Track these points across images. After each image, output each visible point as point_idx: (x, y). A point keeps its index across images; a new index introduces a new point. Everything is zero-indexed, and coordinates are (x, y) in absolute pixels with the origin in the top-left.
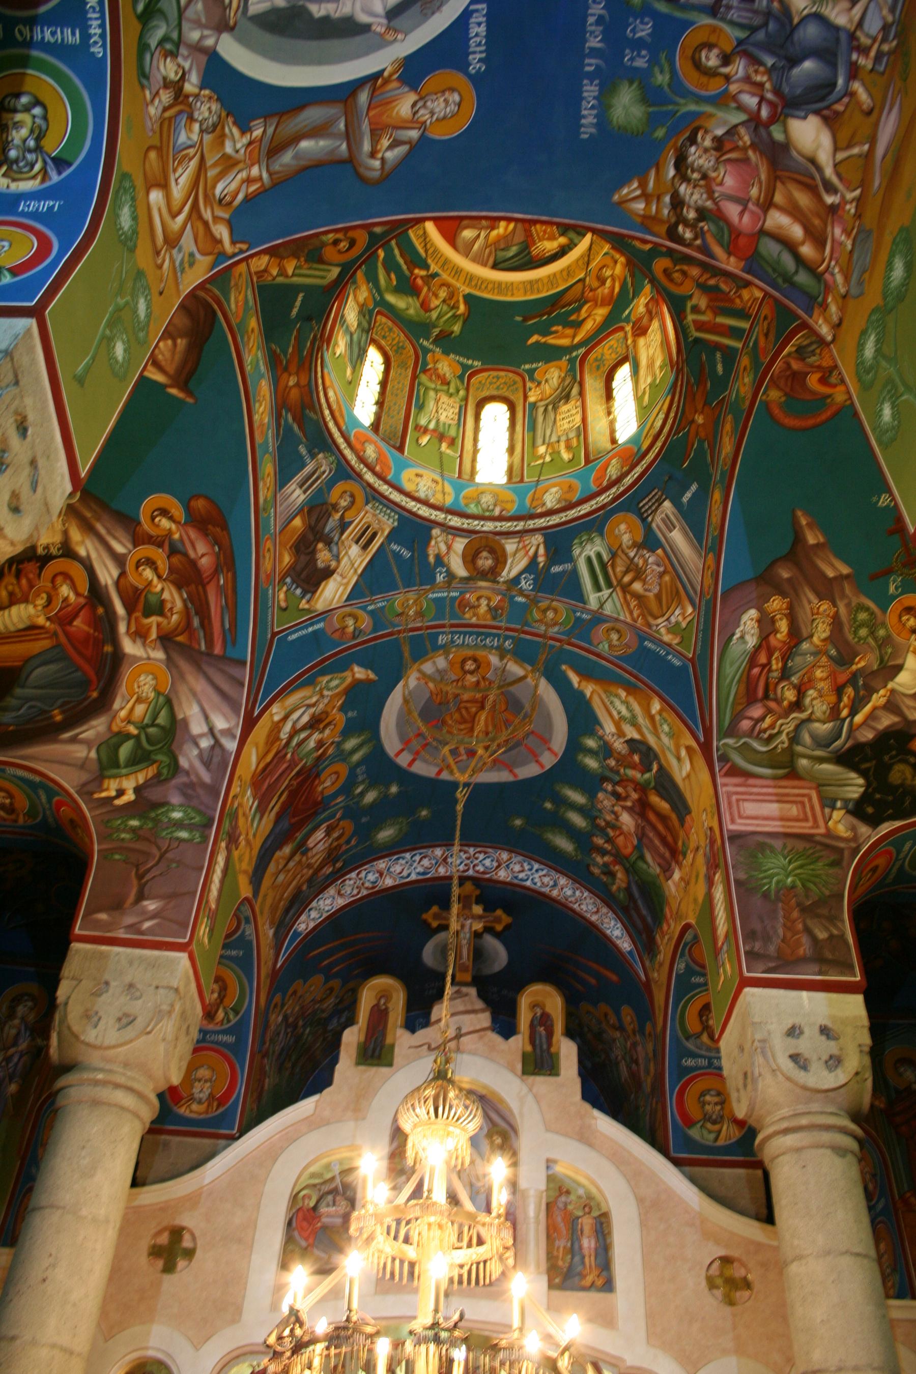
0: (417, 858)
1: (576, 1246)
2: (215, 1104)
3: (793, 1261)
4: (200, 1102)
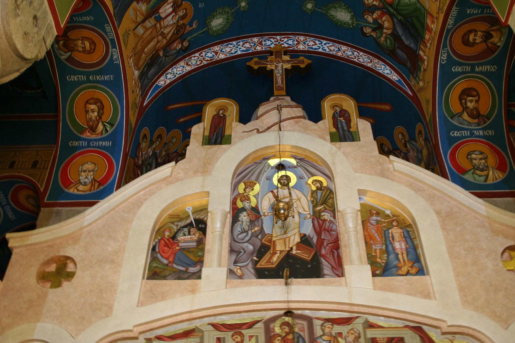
0: (241, 43)
1: (390, 248)
2: (97, 184)
4: (85, 184)
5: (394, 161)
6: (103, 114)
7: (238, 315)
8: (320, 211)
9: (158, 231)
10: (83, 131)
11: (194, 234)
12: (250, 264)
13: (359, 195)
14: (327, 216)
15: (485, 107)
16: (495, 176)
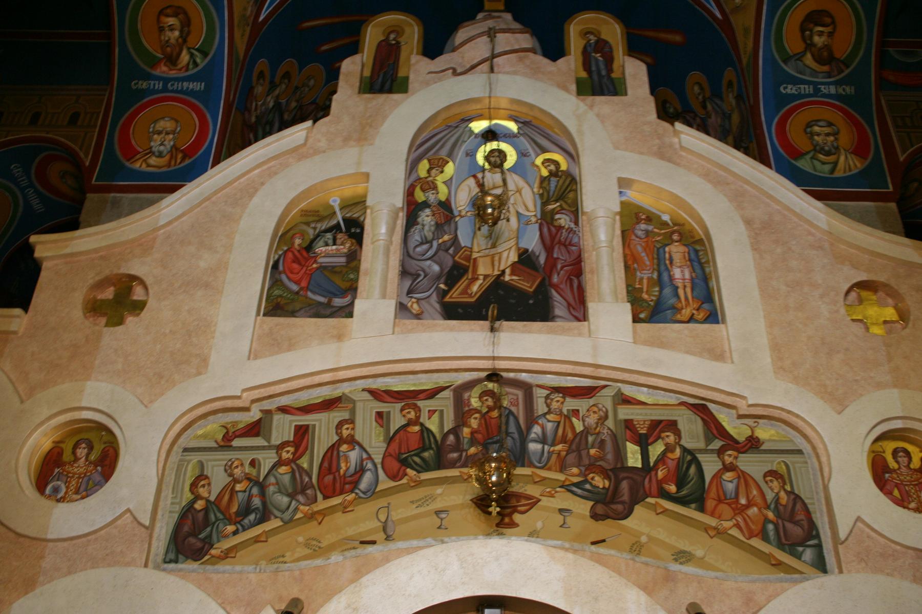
2: (180, 156)
4: (160, 155)
14: (564, 220)
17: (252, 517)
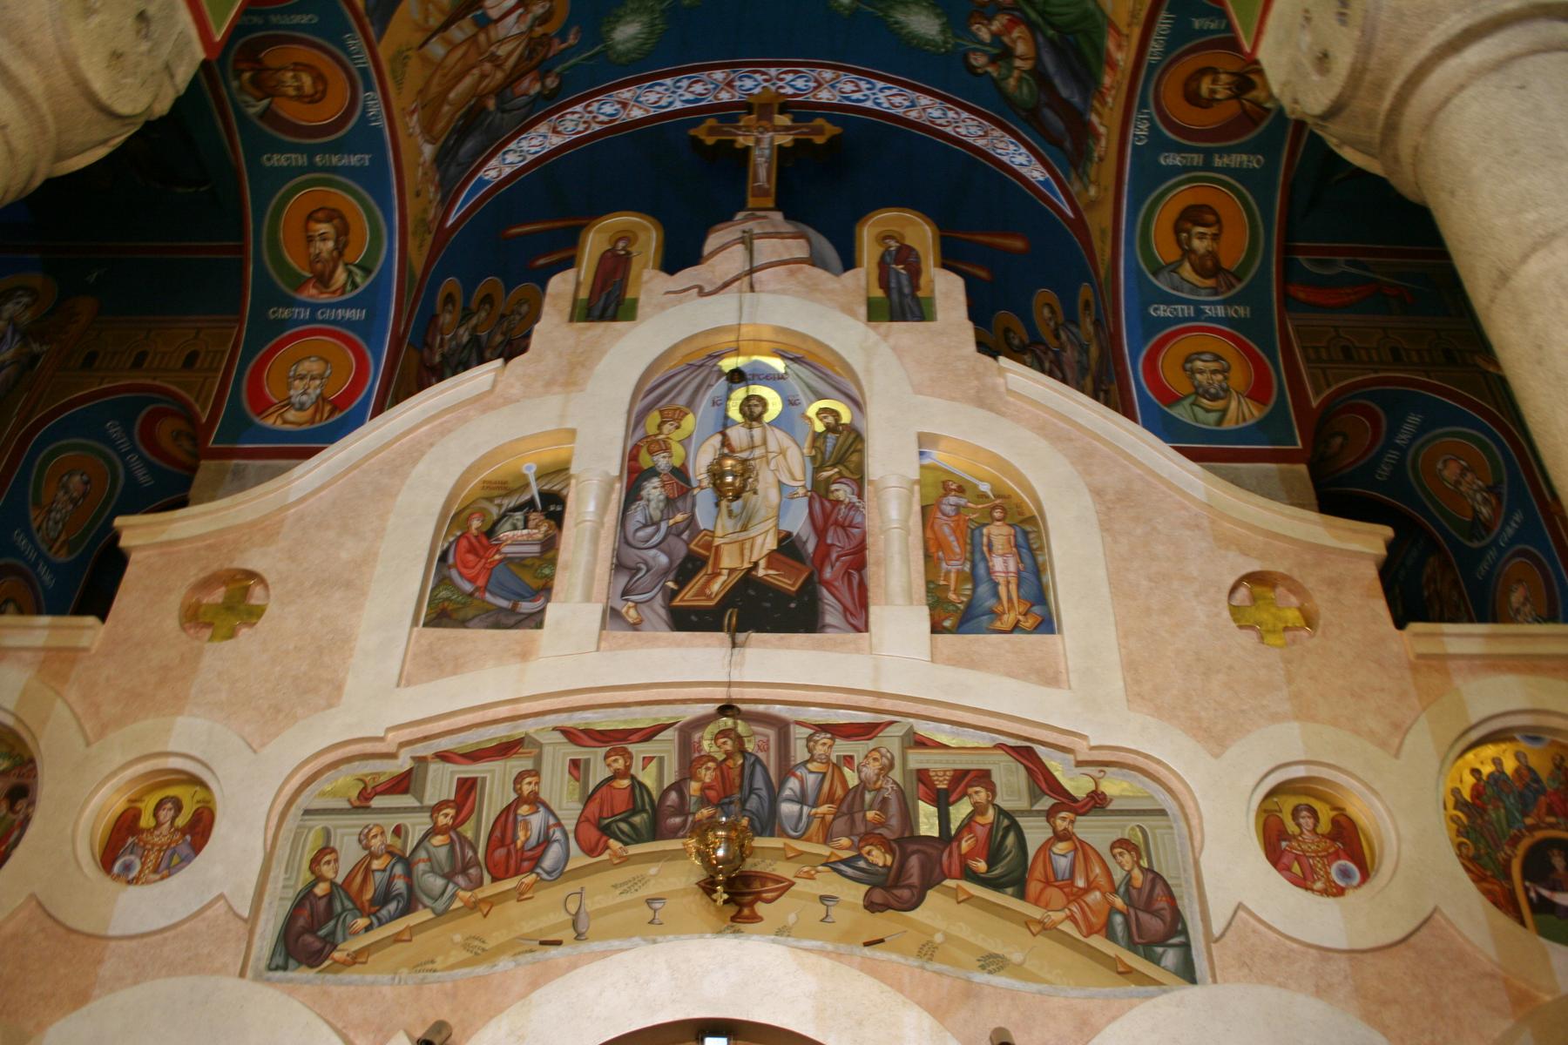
0: (685, 83)
2: (328, 408)
3: (1525, 258)
4: (302, 407)
5: (1009, 370)
6: (346, 245)
7: (621, 710)
8: (829, 481)
9: (456, 518)
10: (300, 284)
11: (537, 527)
12: (659, 597)
13: (920, 446)
14: (843, 492)
15: (1233, 250)
16: (1241, 412)
17: (392, 906)
